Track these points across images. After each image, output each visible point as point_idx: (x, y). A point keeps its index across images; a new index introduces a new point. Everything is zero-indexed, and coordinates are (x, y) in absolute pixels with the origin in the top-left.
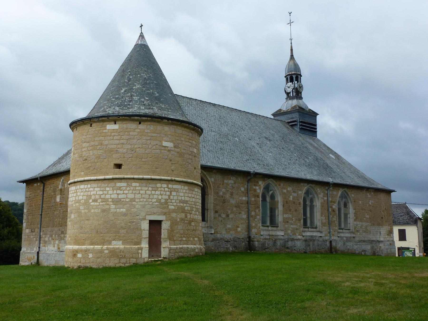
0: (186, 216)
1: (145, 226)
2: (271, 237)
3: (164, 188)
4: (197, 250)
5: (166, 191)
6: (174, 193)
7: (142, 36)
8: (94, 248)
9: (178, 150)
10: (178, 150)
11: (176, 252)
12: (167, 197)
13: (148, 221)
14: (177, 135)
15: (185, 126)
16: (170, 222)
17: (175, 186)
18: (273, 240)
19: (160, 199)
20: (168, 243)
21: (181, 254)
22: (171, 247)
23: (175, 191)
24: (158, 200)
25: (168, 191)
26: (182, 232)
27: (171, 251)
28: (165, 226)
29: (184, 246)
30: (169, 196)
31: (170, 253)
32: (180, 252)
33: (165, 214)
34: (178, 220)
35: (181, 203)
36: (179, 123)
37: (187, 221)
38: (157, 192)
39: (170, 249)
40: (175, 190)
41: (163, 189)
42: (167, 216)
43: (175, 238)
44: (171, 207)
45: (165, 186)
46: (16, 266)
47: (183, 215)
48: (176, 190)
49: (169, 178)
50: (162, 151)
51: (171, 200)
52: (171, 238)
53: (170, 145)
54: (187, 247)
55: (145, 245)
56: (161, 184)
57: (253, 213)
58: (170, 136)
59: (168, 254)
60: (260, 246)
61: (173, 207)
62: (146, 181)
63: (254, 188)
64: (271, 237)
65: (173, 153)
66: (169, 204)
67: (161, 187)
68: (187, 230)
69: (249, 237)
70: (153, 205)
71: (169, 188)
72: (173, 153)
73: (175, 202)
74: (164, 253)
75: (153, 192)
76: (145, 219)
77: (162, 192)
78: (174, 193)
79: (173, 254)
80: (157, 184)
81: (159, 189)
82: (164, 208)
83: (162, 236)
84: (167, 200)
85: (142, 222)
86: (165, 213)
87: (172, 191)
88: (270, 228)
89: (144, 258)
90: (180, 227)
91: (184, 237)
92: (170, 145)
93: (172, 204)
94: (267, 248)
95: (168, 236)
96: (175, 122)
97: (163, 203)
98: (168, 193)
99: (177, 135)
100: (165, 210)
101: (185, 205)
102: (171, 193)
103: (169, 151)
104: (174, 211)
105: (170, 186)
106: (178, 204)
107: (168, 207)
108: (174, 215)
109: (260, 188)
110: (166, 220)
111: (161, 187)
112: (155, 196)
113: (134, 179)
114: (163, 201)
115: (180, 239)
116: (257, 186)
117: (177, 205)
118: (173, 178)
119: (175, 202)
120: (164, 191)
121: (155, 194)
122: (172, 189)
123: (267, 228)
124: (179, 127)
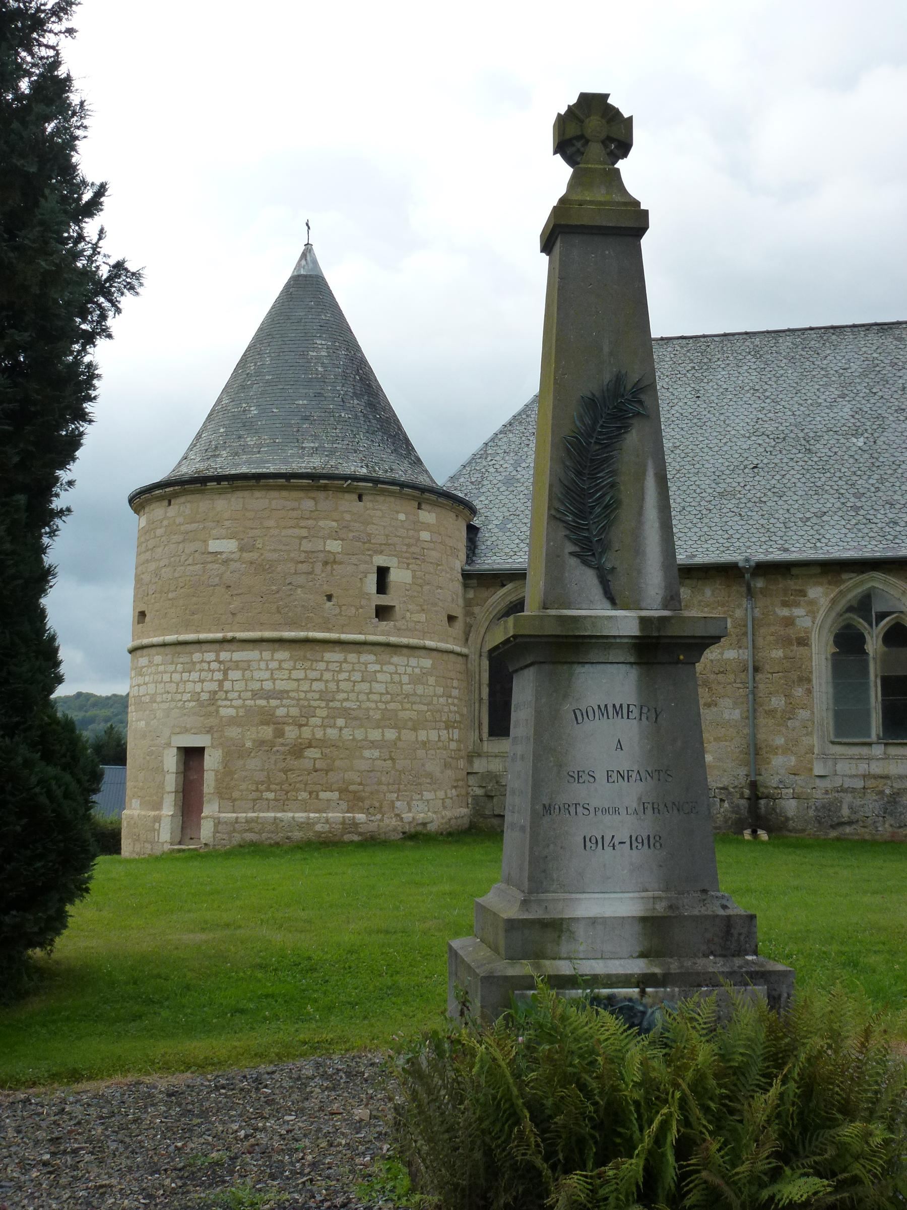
0: (280, 733)
1: (171, 762)
2: (871, 783)
3: (209, 663)
4: (318, 828)
5: (213, 671)
6: (234, 675)
7: (308, 248)
8: (293, 818)
9: (254, 556)
10: (254, 556)
11: (234, 831)
12: (214, 686)
13: (175, 750)
14: (250, 515)
15: (274, 486)
16: (220, 751)
17: (238, 656)
18: (882, 792)
19: (199, 693)
20: (216, 807)
21: (249, 836)
22: (219, 818)
23: (237, 668)
24: (196, 696)
25: (219, 670)
26: (262, 776)
27: (220, 827)
28: (211, 761)
29: (262, 815)
30: (221, 683)
31: (216, 832)
32: (250, 830)
33: (209, 730)
34: (249, 744)
35: (260, 698)
36: (252, 482)
37: (283, 745)
38: (195, 676)
39: (218, 823)
40: (237, 665)
41: (205, 666)
42: (215, 736)
43: (236, 794)
44: (223, 712)
45: (211, 656)
46: (115, 856)
47: (267, 732)
48: (242, 665)
49: (219, 635)
50: (209, 566)
51: (227, 692)
52: (224, 793)
53: (228, 546)
54: (275, 818)
55: (168, 809)
56: (202, 653)
57: (777, 702)
58: (227, 523)
59: (211, 835)
60: (811, 813)
61: (232, 712)
62: (172, 648)
63: (785, 612)
64: (871, 783)
65: (236, 565)
66: (220, 703)
67: (202, 661)
68: (281, 770)
69: (753, 785)
70: (183, 707)
71: (220, 662)
72: (236, 565)
73: (240, 697)
74: (206, 831)
75: (186, 675)
76: (168, 745)
77: (204, 674)
78: (234, 675)
79: (225, 837)
80: (193, 653)
81: (198, 667)
82: (208, 715)
83: (206, 790)
84: (215, 692)
85: (166, 752)
86: (211, 728)
87: (229, 669)
88: (878, 750)
89: (163, 844)
90: (253, 763)
91: (268, 789)
92: (228, 546)
93: (228, 703)
94: (850, 823)
95: (217, 788)
96: (239, 483)
97: (206, 703)
98: (219, 676)
99: (250, 515)
100: (212, 721)
101: (274, 703)
102: (225, 674)
103: (226, 562)
104: (233, 721)
105: (224, 656)
106: (248, 702)
107: (217, 711)
108: (233, 732)
109: (812, 614)
110: (213, 746)
111: (202, 661)
112: (189, 686)
113: (199, 642)
114: (205, 696)
115: (255, 795)
116: (797, 605)
117: (243, 706)
118: (230, 635)
119: (240, 697)
120: (209, 670)
121: (189, 681)
122: (228, 665)
123: (864, 751)
124: (257, 494)
